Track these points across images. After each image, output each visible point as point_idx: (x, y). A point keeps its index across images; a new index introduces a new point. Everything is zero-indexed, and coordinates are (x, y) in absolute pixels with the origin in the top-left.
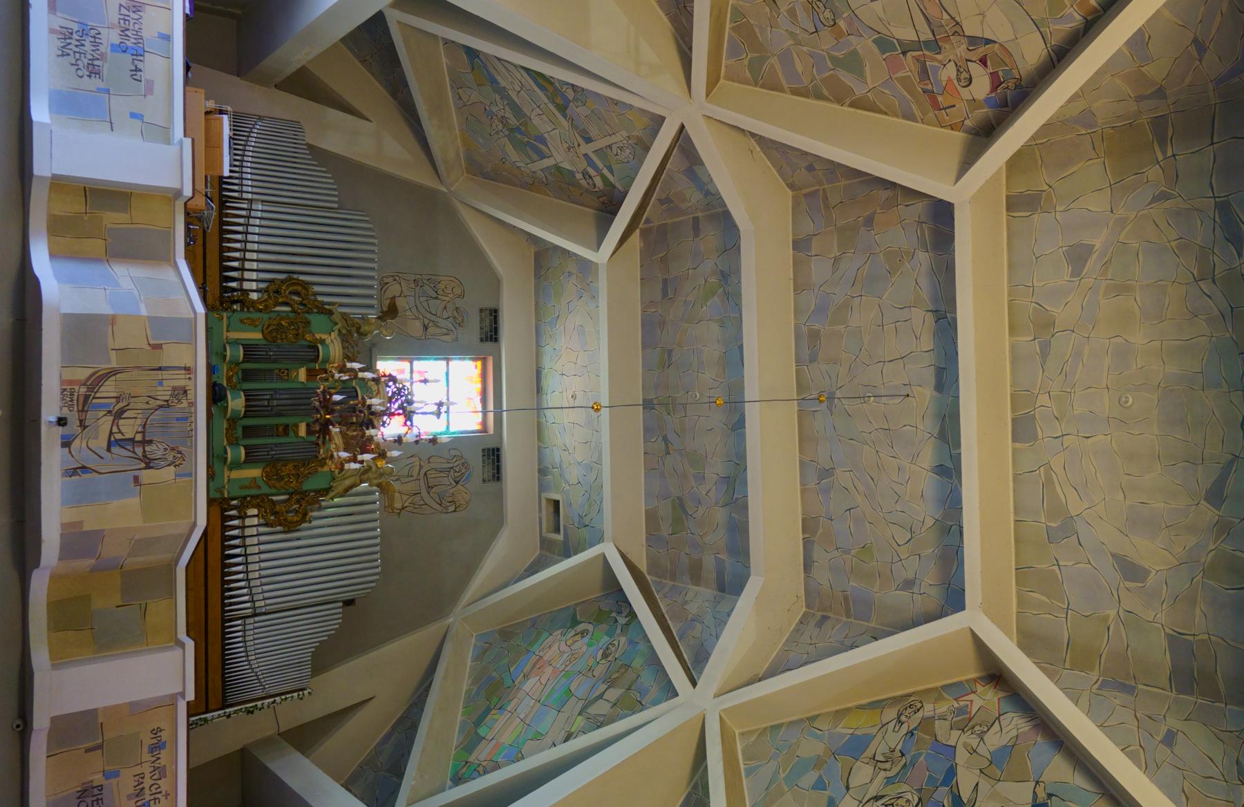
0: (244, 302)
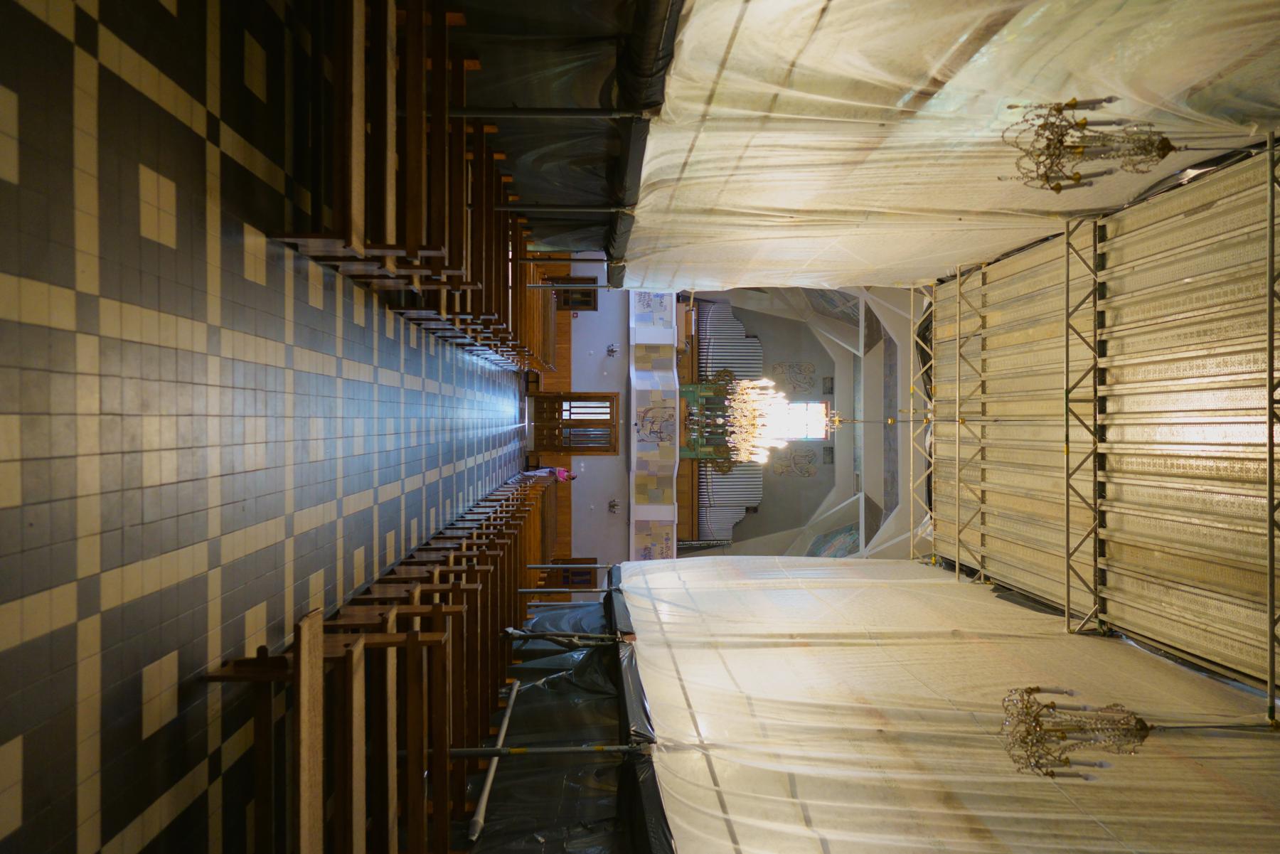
0: (707, 380)
